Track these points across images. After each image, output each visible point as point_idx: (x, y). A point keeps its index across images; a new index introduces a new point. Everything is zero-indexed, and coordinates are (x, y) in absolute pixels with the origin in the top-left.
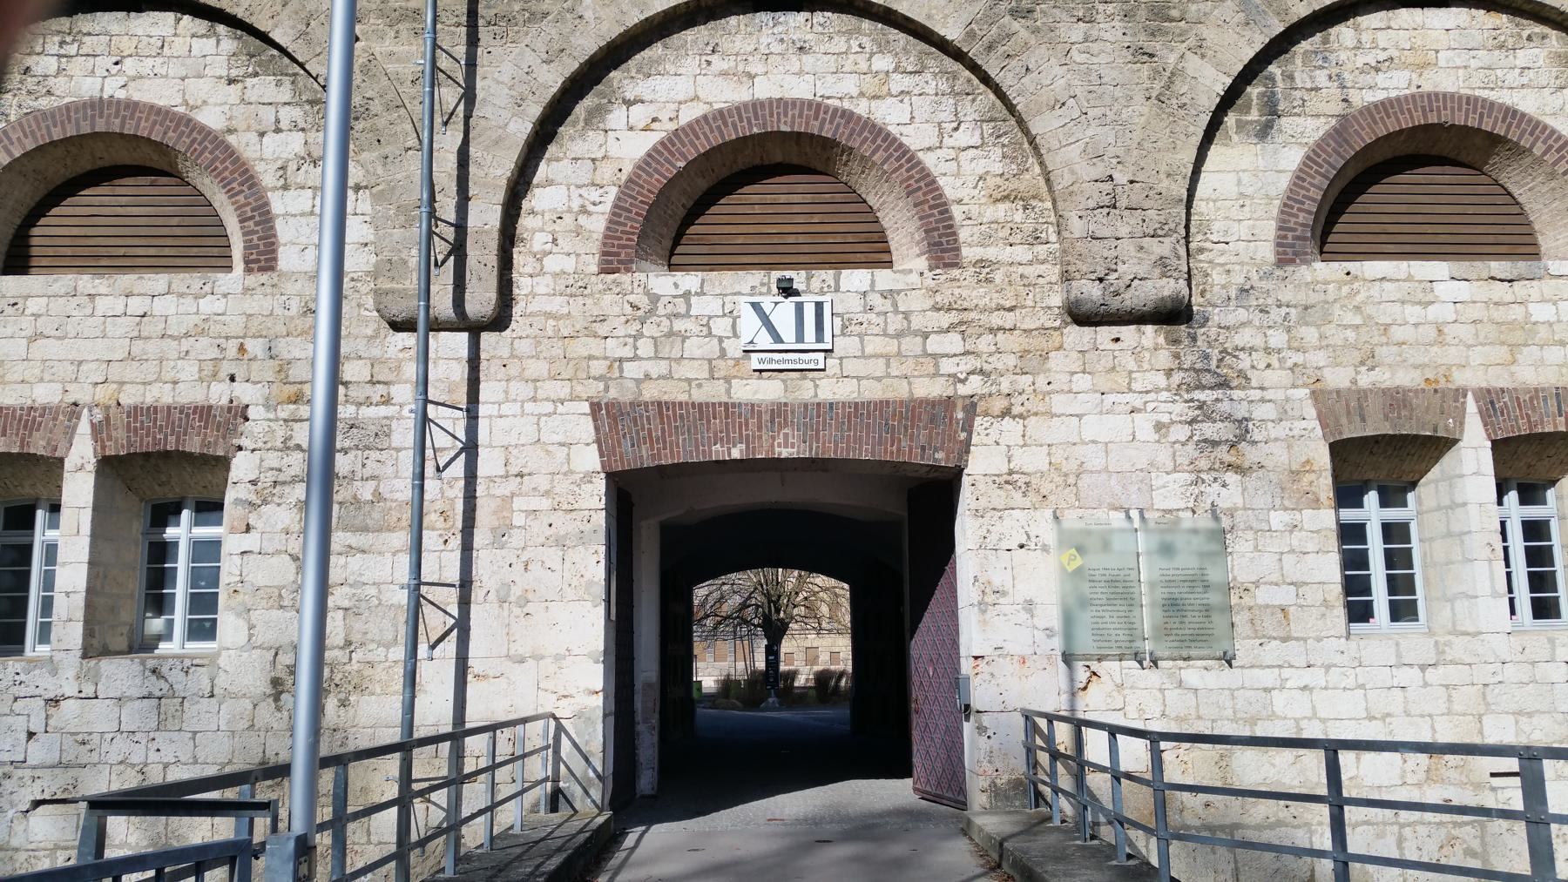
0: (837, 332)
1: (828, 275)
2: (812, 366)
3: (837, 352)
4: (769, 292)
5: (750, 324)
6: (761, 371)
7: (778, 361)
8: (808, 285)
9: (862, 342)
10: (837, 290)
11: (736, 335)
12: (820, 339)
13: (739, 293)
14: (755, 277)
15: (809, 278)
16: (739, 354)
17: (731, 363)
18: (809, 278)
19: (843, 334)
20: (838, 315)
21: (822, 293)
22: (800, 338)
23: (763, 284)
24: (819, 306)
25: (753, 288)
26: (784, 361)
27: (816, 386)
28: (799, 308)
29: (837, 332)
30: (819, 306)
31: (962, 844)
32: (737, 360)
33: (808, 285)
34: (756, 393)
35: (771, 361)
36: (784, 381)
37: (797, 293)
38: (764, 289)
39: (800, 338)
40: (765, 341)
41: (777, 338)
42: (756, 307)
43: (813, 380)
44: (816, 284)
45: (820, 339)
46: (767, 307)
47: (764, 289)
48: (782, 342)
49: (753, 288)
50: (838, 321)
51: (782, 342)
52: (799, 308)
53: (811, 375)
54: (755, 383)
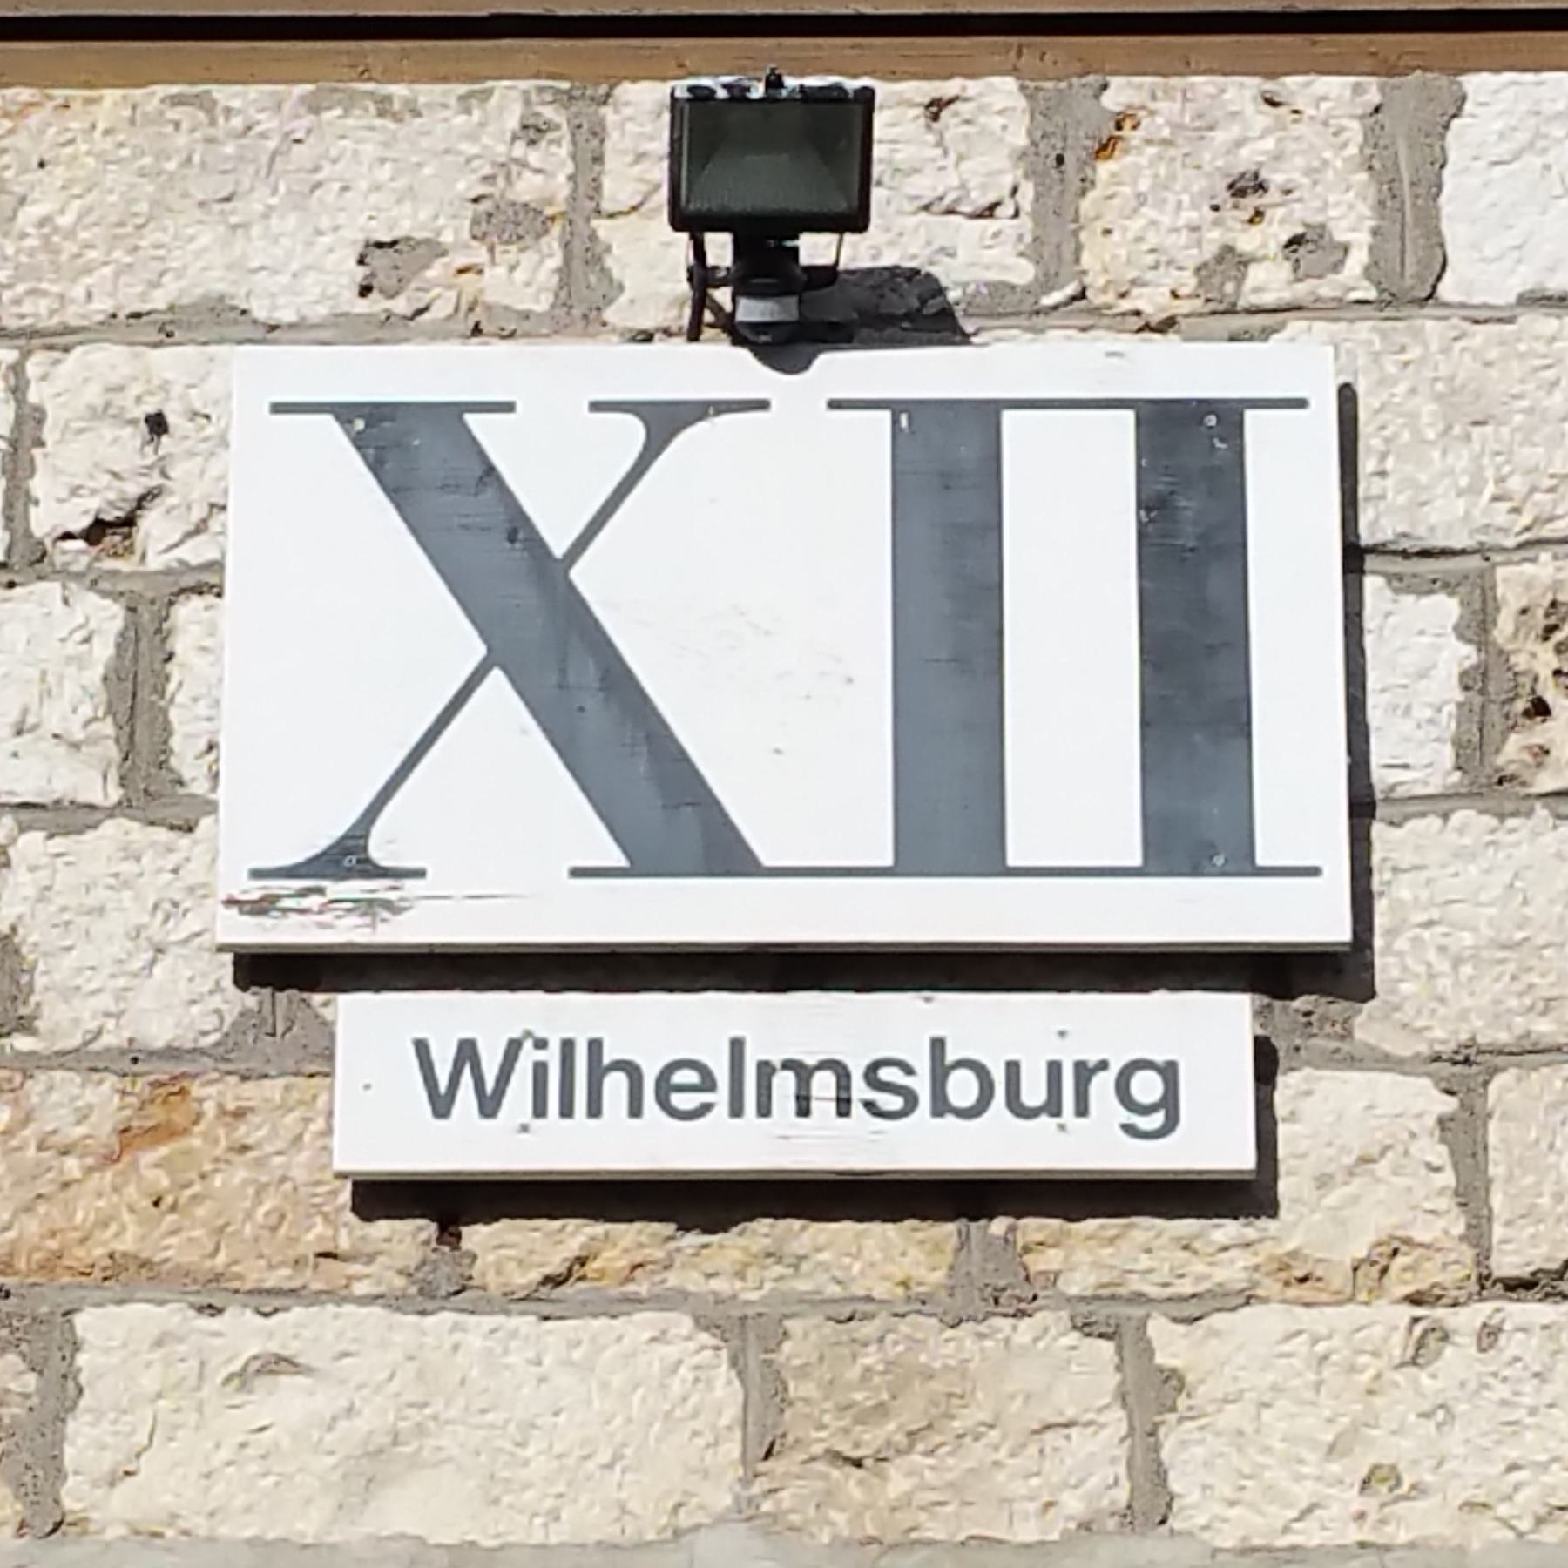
0: (1414, 751)
1: (1309, 124)
2: (1095, 1144)
3: (1425, 985)
4: (581, 305)
5: (330, 674)
6: (450, 1202)
7: (681, 1084)
8: (1056, 243)
9: (1464, 1134)
10: (1409, 284)
11: (154, 785)
12: (1194, 815)
13: (222, 320)
14: (425, 147)
15: (1063, 164)
16: (188, 1000)
17: (85, 1106)
18: (1063, 164)
19: (1486, 785)
20: (1421, 562)
21: (1225, 310)
22: (951, 797)
23: (505, 223)
24: (1189, 465)
25: (385, 259)
26: (751, 1084)
27: (1154, 1394)
28: (949, 484)
29: (1414, 751)
30: (1189, 465)
31: (1074, 1285)
32: (162, 1082)
33: (1056, 243)
34: (374, 1466)
35: (580, 1078)
36: (741, 1332)
37: (911, 310)
38: (525, 278)
39: (951, 797)
40: (510, 843)
41: (666, 809)
42: (418, 455)
43: (1107, 1318)
44: (1146, 217)
45: (1194, 815)
46: (551, 456)
47: (525, 278)
48: (726, 854)
49: (385, 259)
50: (1420, 642)
51: (726, 854)
52: (949, 484)
53: (1083, 1253)
54: (372, 1350)
